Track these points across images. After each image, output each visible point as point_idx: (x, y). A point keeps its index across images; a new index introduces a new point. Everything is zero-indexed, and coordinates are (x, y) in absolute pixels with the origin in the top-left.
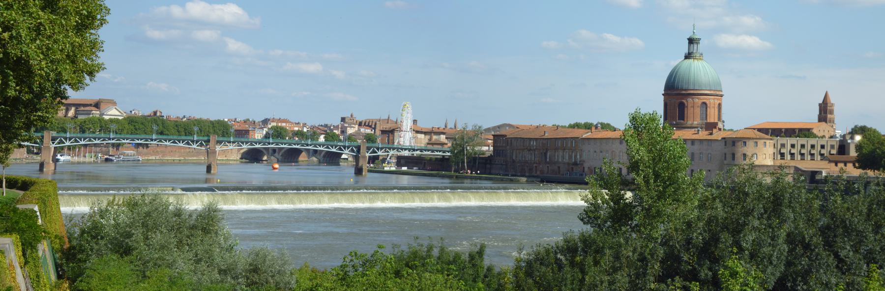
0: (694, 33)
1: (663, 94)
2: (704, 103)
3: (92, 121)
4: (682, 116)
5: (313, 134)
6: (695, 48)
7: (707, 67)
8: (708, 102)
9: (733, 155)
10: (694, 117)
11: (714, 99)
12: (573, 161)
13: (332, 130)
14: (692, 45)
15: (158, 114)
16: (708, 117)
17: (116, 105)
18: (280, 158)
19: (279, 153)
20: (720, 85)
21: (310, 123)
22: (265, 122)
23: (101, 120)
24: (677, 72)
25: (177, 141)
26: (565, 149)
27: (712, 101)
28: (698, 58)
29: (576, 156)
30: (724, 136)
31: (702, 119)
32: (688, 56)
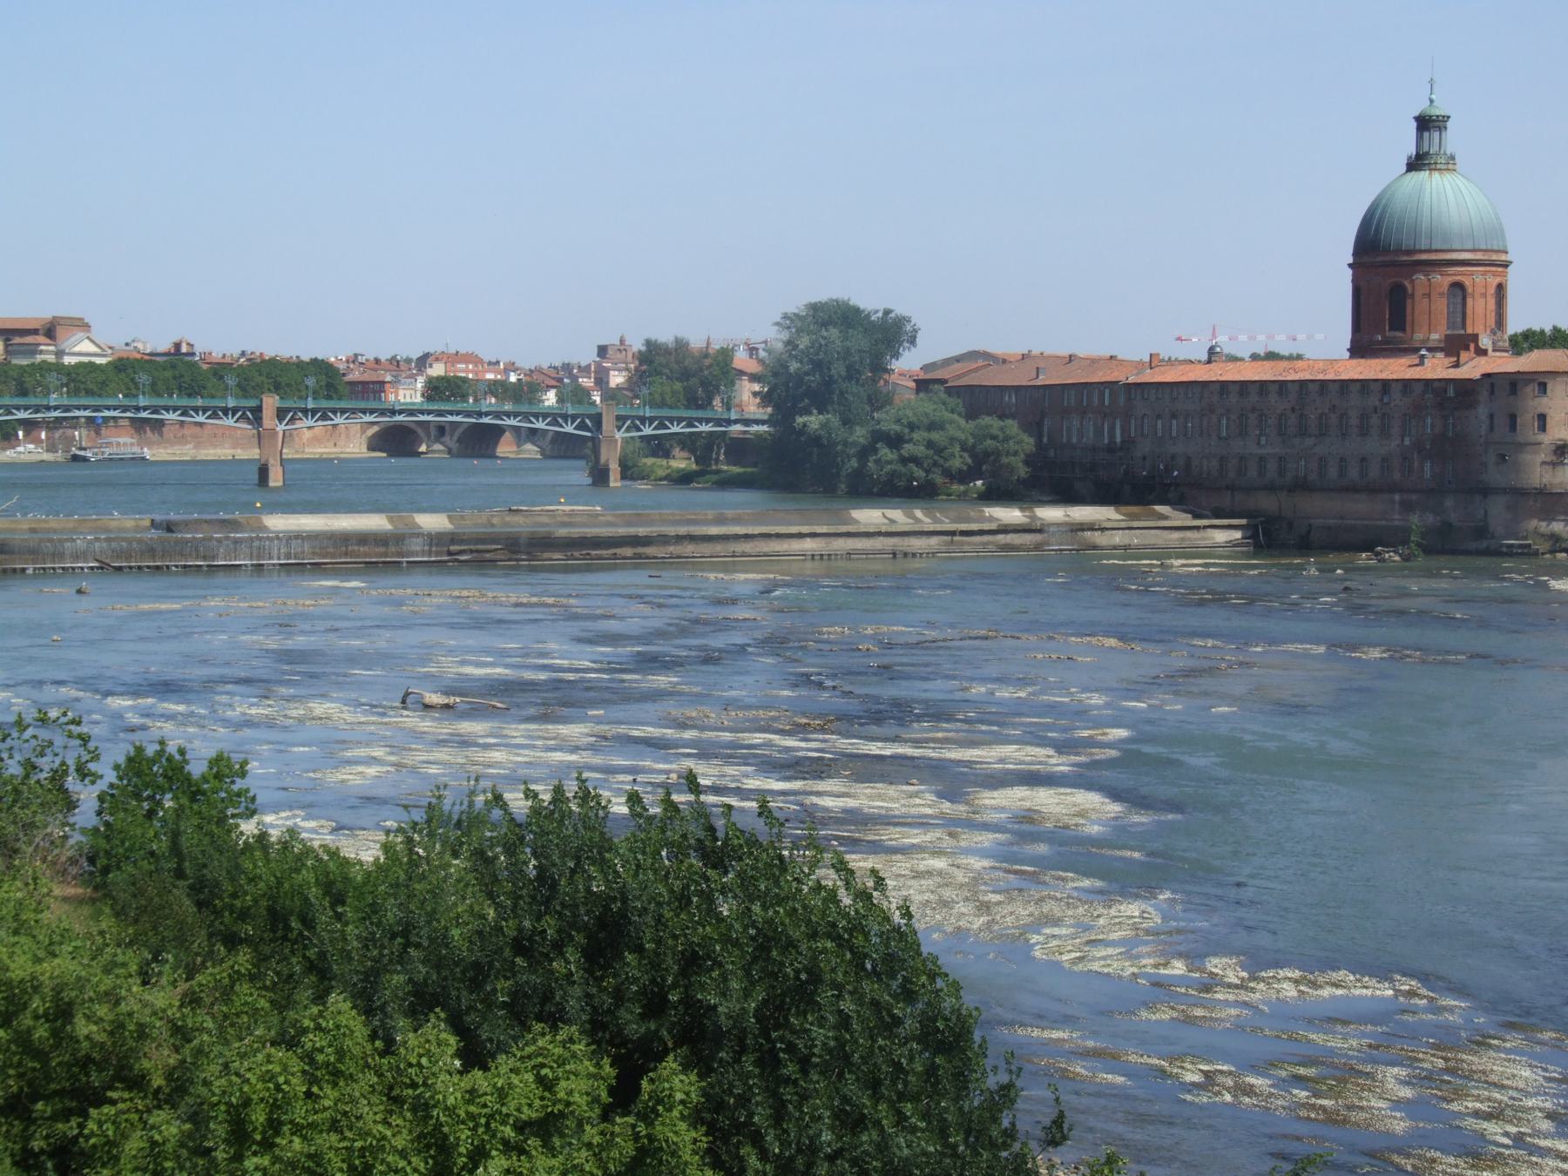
0: (1432, 101)
1: (1350, 265)
2: (1458, 286)
3: (45, 367)
4: (1399, 320)
5: (525, 392)
6: (1437, 141)
7: (1463, 188)
8: (1467, 282)
9: (1513, 418)
10: (1431, 322)
11: (1485, 273)
12: (1106, 441)
13: (574, 378)
14: (1426, 135)
15: (184, 349)
16: (1469, 322)
17: (89, 331)
18: (454, 446)
19: (452, 436)
20: (1499, 232)
21: (527, 363)
22: (423, 361)
23: (59, 368)
24: (1385, 206)
25: (560, 420)
26: (1085, 412)
27: (1477, 281)
28: (1443, 167)
29: (1112, 429)
30: (1489, 371)
31: (1451, 325)
32: (1417, 163)
